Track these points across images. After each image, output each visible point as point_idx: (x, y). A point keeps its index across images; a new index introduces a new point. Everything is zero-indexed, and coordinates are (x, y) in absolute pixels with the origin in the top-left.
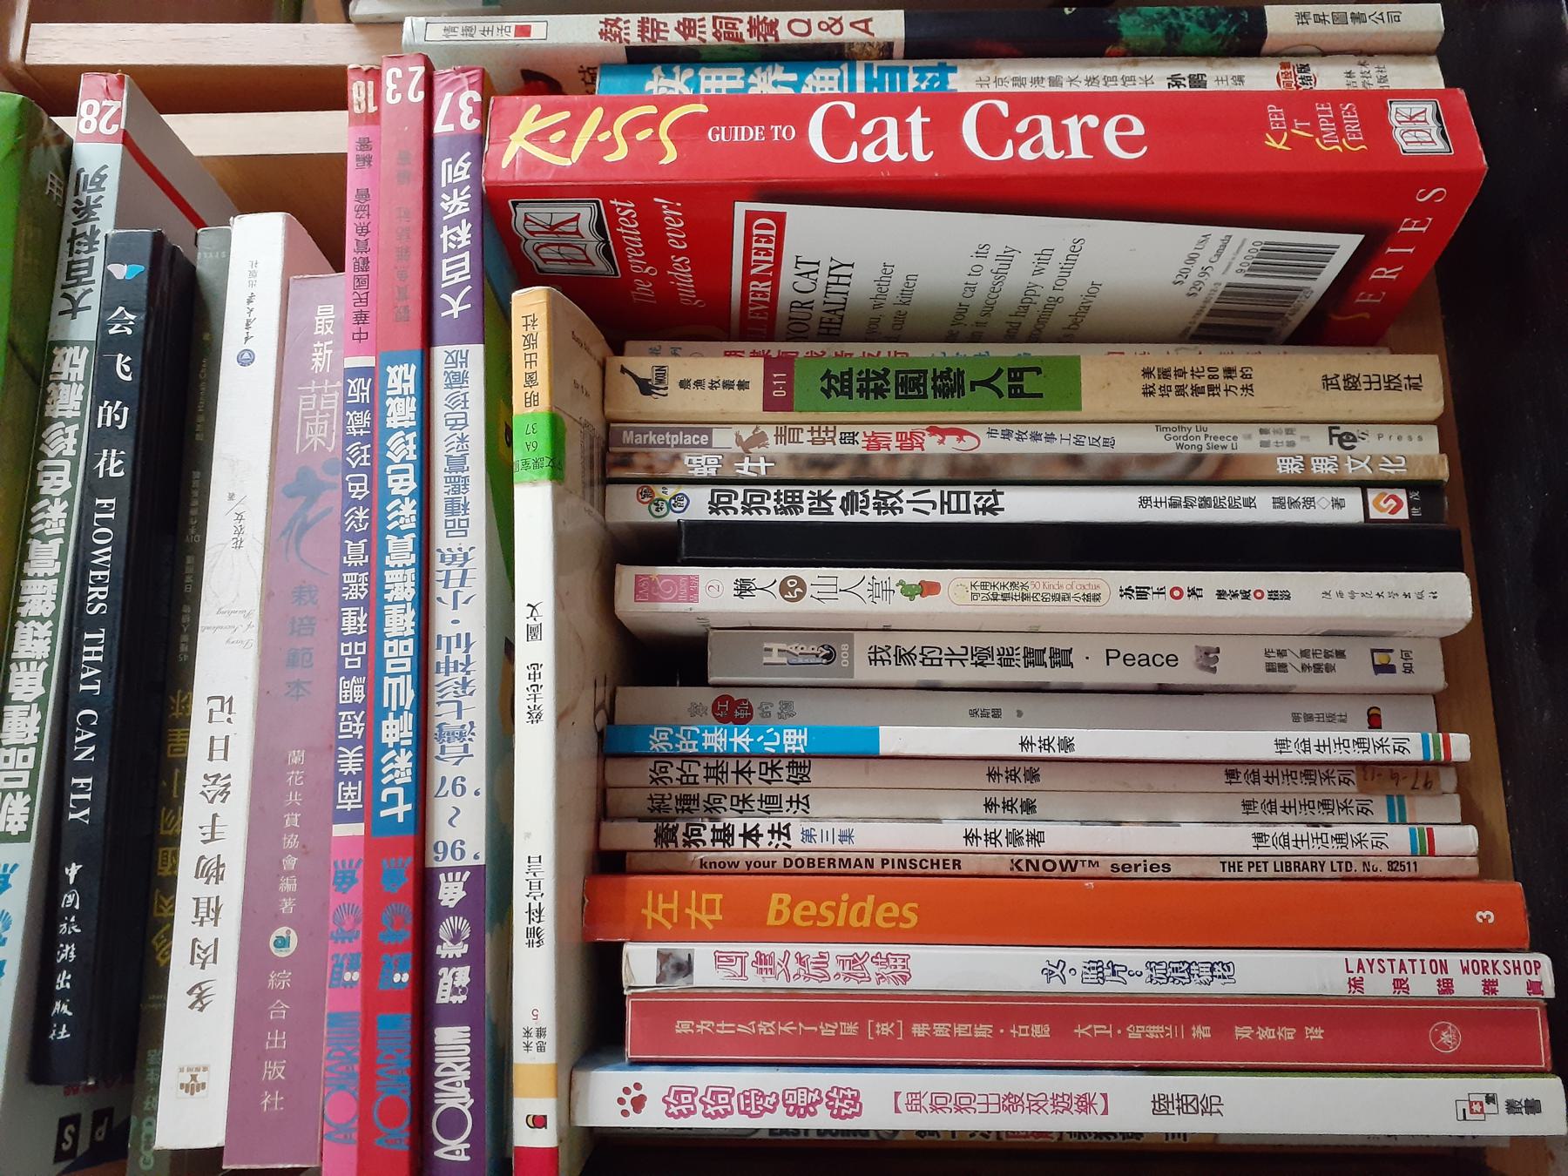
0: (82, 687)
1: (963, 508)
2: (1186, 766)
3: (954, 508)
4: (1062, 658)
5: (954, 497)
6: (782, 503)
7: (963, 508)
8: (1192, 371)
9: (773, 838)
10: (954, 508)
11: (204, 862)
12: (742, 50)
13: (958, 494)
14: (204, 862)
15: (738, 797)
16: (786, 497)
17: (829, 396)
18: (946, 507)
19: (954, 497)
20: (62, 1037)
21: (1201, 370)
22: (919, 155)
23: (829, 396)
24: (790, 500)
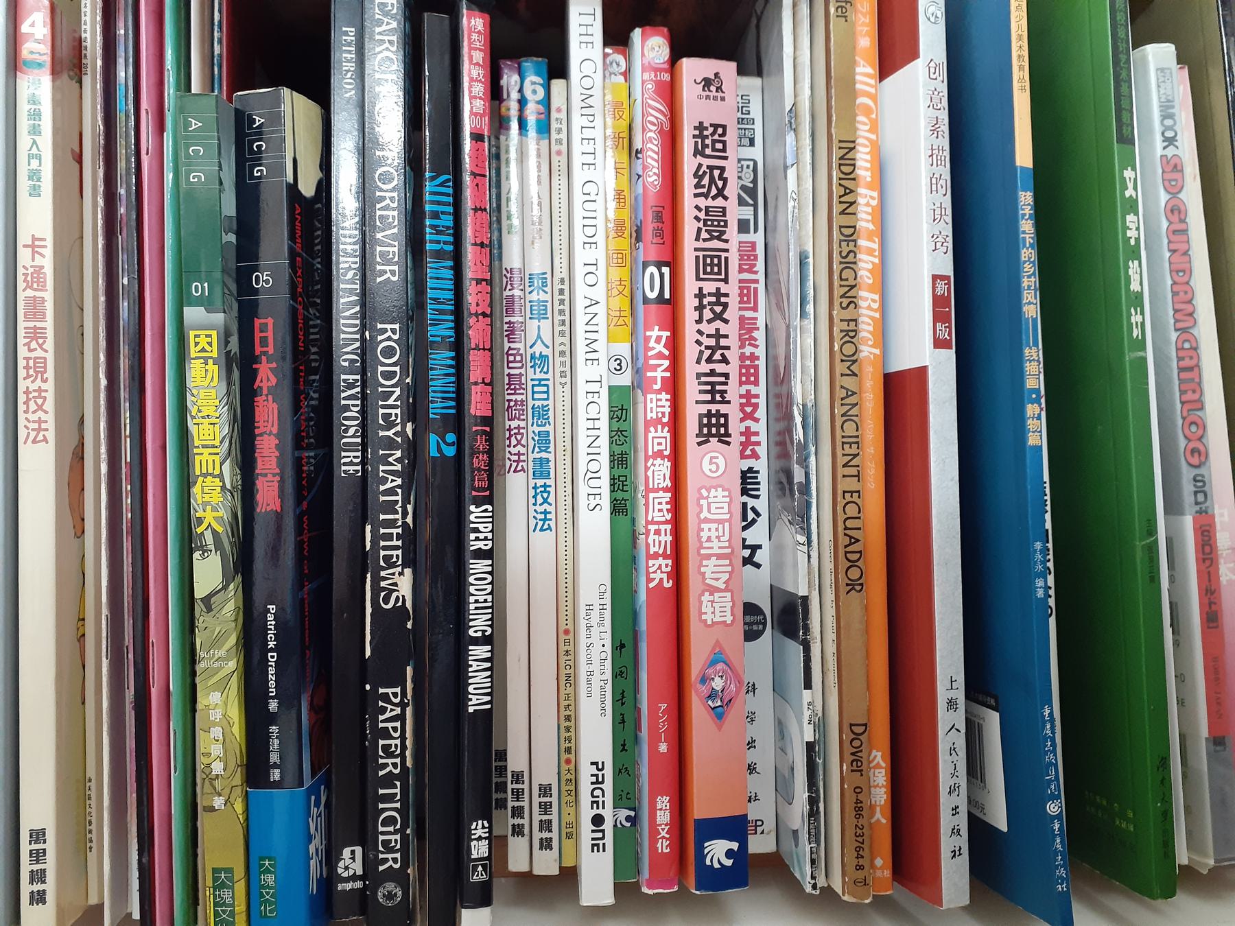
0: (383, 498)
1: (536, 396)
3: (536, 389)
5: (545, 389)
7: (536, 396)
9: (708, 336)
10: (536, 389)
12: (1209, 99)
13: (547, 392)
15: (626, 481)
18: (537, 383)
19: (545, 389)
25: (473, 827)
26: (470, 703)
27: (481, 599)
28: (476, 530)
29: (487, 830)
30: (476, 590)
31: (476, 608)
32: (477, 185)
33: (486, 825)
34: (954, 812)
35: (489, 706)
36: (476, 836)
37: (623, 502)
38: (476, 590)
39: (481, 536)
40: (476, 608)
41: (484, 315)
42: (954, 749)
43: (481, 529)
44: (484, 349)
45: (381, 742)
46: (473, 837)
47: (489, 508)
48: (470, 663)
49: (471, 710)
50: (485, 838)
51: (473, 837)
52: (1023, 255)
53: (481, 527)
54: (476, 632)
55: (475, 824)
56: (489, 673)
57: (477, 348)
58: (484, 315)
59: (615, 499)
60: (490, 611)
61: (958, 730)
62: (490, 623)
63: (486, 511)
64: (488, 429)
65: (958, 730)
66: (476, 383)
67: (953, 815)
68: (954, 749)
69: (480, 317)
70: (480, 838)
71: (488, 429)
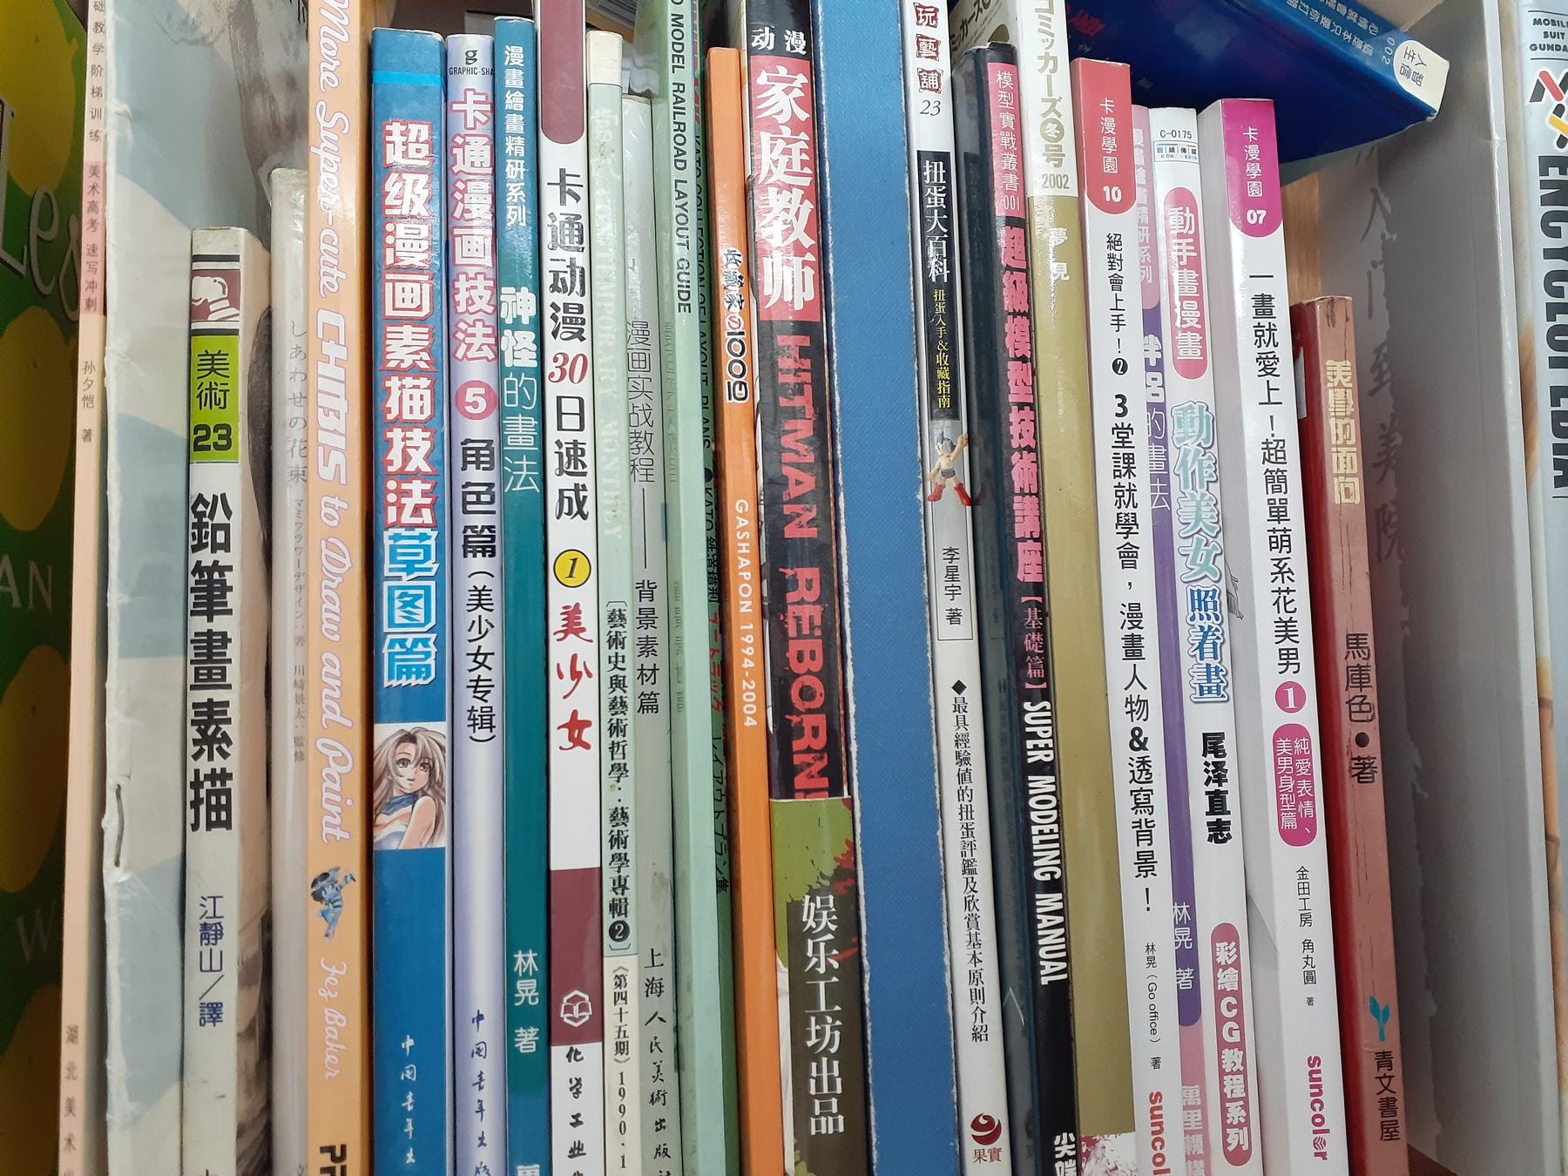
2: (458, 1143)
4: (1218, 832)
6: (207, 785)
8: (1288, 591)
11: (1144, 716)
14: (1144, 716)
16: (218, 793)
17: (573, 1117)
20: (518, 488)
21: (1289, 608)
22: (751, 627)
23: (573, 1117)
24: (213, 800)
25: (1056, 1143)
26: (1043, 972)
27: (1046, 829)
28: (1034, 736)
29: (1073, 1146)
30: (1040, 817)
31: (1042, 842)
32: (1015, 282)
33: (1073, 1139)
34: (659, 1126)
35: (1064, 976)
36: (1061, 1155)
37: (652, 697)
38: (1040, 817)
39: (1041, 743)
40: (1042, 842)
41: (1029, 449)
42: (656, 1044)
43: (1041, 734)
44: (1031, 494)
45: (343, 973)
46: (1057, 1156)
47: (1047, 704)
48: (1039, 917)
49: (1044, 981)
50: (1072, 1157)
51: (1057, 1156)
52: (1014, 430)
53: (1039, 731)
54: (1043, 874)
55: (1058, 1138)
56: (1061, 931)
57: (1023, 494)
58: (1029, 449)
59: (642, 694)
60: (1057, 845)
61: (661, 1019)
62: (1058, 862)
63: (1044, 709)
64: (1040, 599)
65: (661, 1019)
66: (1024, 540)
67: (657, 1130)
68: (656, 1044)
69: (1025, 453)
70: (1066, 1158)
71: (1040, 599)
